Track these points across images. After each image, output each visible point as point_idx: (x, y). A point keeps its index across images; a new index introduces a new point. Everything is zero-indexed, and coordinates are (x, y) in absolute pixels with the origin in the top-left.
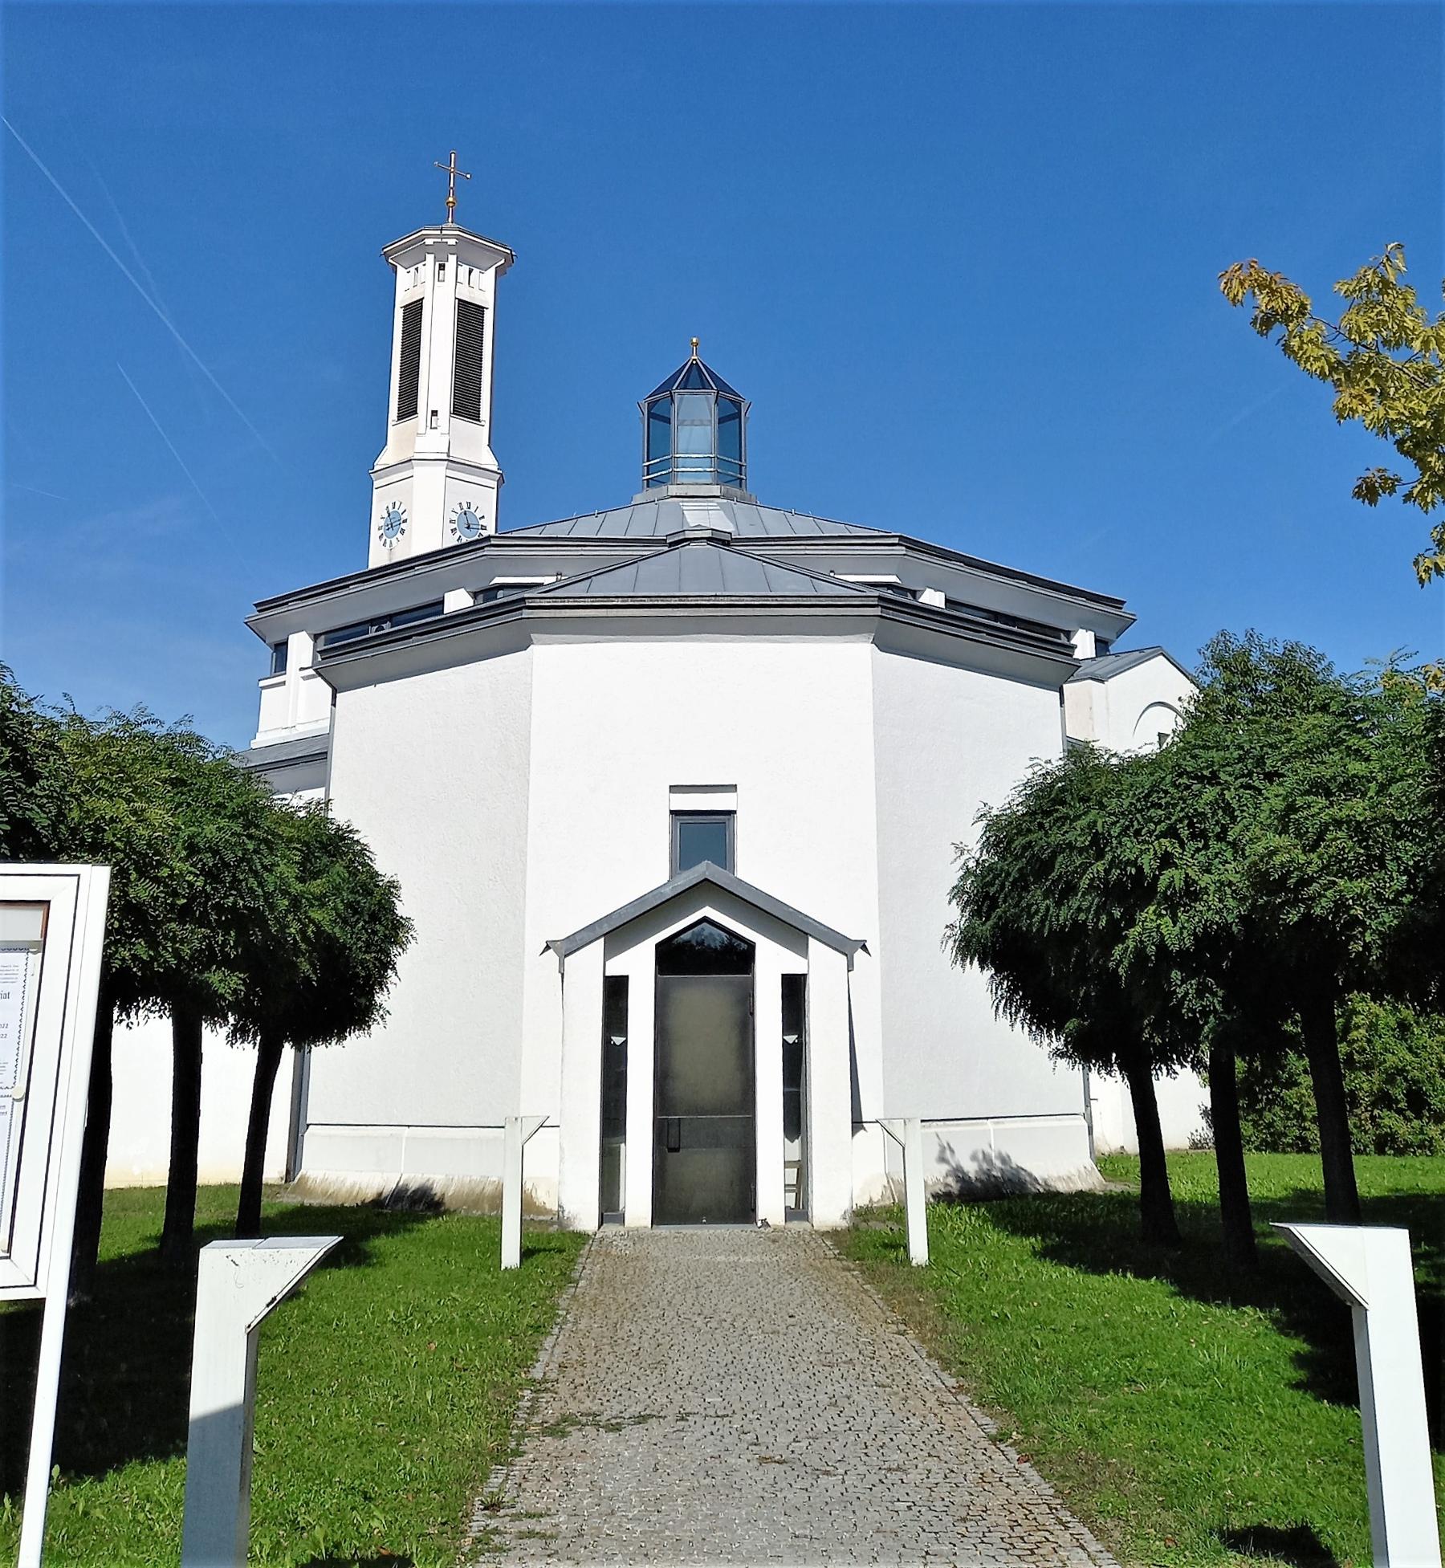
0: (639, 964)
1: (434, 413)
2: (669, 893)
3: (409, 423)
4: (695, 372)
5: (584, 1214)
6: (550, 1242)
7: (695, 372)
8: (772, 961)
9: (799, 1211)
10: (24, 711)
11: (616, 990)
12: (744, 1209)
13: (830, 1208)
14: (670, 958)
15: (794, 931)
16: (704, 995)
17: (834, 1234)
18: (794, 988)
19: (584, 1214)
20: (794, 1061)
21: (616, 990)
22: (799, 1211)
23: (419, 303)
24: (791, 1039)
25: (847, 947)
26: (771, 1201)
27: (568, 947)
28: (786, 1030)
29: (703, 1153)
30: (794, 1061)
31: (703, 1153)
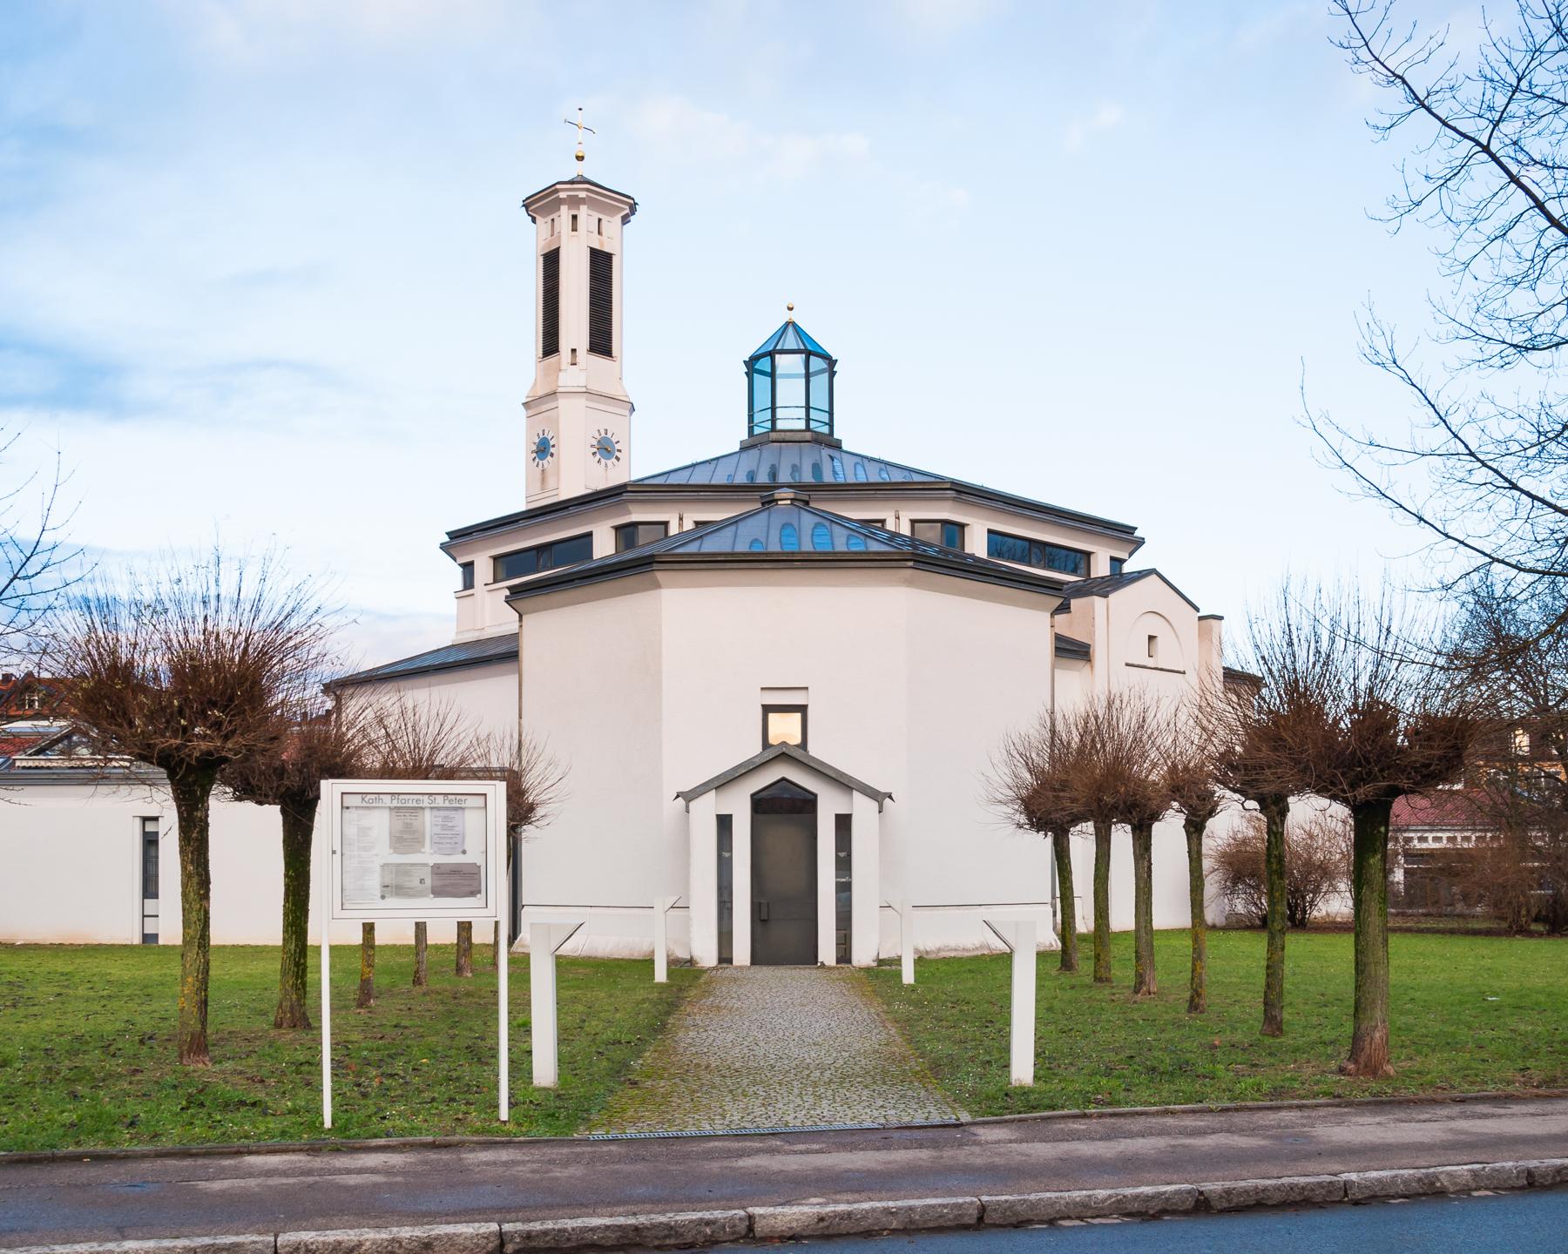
0: (739, 806)
1: (574, 351)
2: (758, 761)
3: (552, 359)
4: (790, 329)
5: (707, 955)
6: (684, 969)
7: (790, 329)
8: (829, 806)
9: (844, 955)
10: (83, 725)
11: (724, 823)
12: (808, 955)
13: (863, 955)
14: (762, 805)
15: (844, 784)
16: (784, 835)
17: (868, 970)
18: (843, 823)
19: (707, 955)
20: (844, 889)
21: (724, 823)
22: (844, 955)
23: (557, 251)
24: (842, 854)
25: (878, 797)
26: (827, 951)
27: (689, 796)
28: (838, 850)
29: (784, 921)
30: (844, 889)
31: (784, 921)
